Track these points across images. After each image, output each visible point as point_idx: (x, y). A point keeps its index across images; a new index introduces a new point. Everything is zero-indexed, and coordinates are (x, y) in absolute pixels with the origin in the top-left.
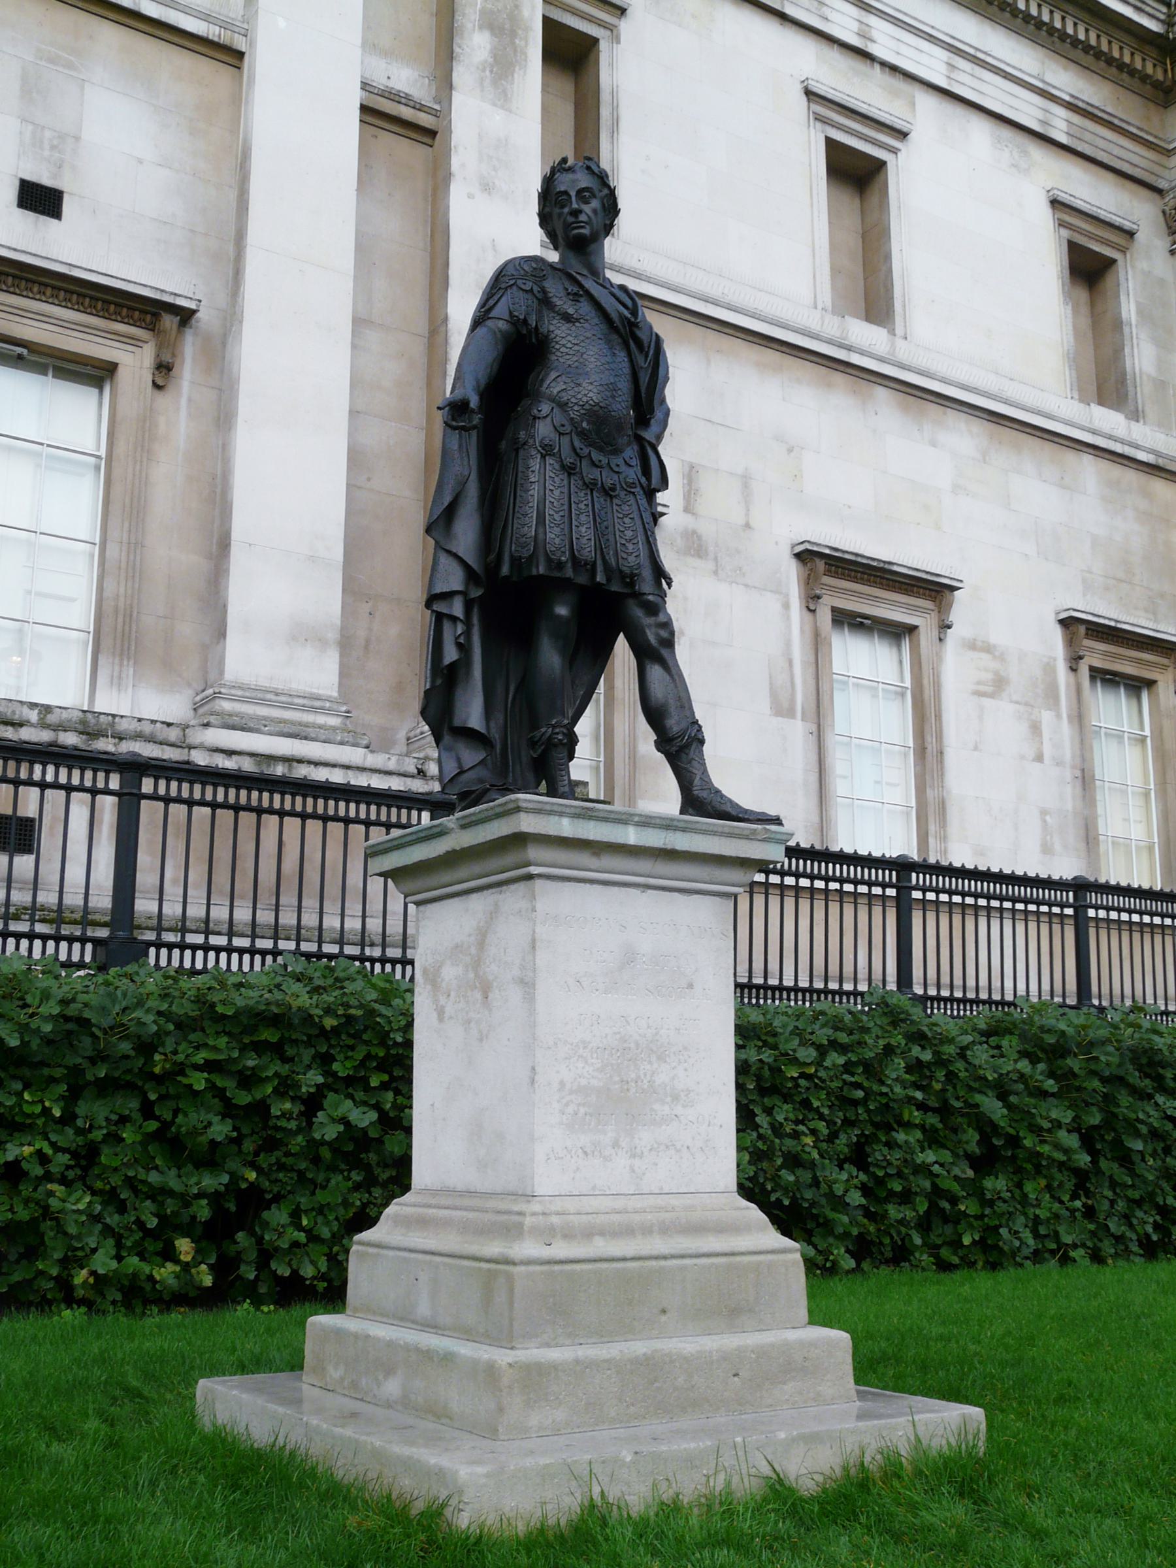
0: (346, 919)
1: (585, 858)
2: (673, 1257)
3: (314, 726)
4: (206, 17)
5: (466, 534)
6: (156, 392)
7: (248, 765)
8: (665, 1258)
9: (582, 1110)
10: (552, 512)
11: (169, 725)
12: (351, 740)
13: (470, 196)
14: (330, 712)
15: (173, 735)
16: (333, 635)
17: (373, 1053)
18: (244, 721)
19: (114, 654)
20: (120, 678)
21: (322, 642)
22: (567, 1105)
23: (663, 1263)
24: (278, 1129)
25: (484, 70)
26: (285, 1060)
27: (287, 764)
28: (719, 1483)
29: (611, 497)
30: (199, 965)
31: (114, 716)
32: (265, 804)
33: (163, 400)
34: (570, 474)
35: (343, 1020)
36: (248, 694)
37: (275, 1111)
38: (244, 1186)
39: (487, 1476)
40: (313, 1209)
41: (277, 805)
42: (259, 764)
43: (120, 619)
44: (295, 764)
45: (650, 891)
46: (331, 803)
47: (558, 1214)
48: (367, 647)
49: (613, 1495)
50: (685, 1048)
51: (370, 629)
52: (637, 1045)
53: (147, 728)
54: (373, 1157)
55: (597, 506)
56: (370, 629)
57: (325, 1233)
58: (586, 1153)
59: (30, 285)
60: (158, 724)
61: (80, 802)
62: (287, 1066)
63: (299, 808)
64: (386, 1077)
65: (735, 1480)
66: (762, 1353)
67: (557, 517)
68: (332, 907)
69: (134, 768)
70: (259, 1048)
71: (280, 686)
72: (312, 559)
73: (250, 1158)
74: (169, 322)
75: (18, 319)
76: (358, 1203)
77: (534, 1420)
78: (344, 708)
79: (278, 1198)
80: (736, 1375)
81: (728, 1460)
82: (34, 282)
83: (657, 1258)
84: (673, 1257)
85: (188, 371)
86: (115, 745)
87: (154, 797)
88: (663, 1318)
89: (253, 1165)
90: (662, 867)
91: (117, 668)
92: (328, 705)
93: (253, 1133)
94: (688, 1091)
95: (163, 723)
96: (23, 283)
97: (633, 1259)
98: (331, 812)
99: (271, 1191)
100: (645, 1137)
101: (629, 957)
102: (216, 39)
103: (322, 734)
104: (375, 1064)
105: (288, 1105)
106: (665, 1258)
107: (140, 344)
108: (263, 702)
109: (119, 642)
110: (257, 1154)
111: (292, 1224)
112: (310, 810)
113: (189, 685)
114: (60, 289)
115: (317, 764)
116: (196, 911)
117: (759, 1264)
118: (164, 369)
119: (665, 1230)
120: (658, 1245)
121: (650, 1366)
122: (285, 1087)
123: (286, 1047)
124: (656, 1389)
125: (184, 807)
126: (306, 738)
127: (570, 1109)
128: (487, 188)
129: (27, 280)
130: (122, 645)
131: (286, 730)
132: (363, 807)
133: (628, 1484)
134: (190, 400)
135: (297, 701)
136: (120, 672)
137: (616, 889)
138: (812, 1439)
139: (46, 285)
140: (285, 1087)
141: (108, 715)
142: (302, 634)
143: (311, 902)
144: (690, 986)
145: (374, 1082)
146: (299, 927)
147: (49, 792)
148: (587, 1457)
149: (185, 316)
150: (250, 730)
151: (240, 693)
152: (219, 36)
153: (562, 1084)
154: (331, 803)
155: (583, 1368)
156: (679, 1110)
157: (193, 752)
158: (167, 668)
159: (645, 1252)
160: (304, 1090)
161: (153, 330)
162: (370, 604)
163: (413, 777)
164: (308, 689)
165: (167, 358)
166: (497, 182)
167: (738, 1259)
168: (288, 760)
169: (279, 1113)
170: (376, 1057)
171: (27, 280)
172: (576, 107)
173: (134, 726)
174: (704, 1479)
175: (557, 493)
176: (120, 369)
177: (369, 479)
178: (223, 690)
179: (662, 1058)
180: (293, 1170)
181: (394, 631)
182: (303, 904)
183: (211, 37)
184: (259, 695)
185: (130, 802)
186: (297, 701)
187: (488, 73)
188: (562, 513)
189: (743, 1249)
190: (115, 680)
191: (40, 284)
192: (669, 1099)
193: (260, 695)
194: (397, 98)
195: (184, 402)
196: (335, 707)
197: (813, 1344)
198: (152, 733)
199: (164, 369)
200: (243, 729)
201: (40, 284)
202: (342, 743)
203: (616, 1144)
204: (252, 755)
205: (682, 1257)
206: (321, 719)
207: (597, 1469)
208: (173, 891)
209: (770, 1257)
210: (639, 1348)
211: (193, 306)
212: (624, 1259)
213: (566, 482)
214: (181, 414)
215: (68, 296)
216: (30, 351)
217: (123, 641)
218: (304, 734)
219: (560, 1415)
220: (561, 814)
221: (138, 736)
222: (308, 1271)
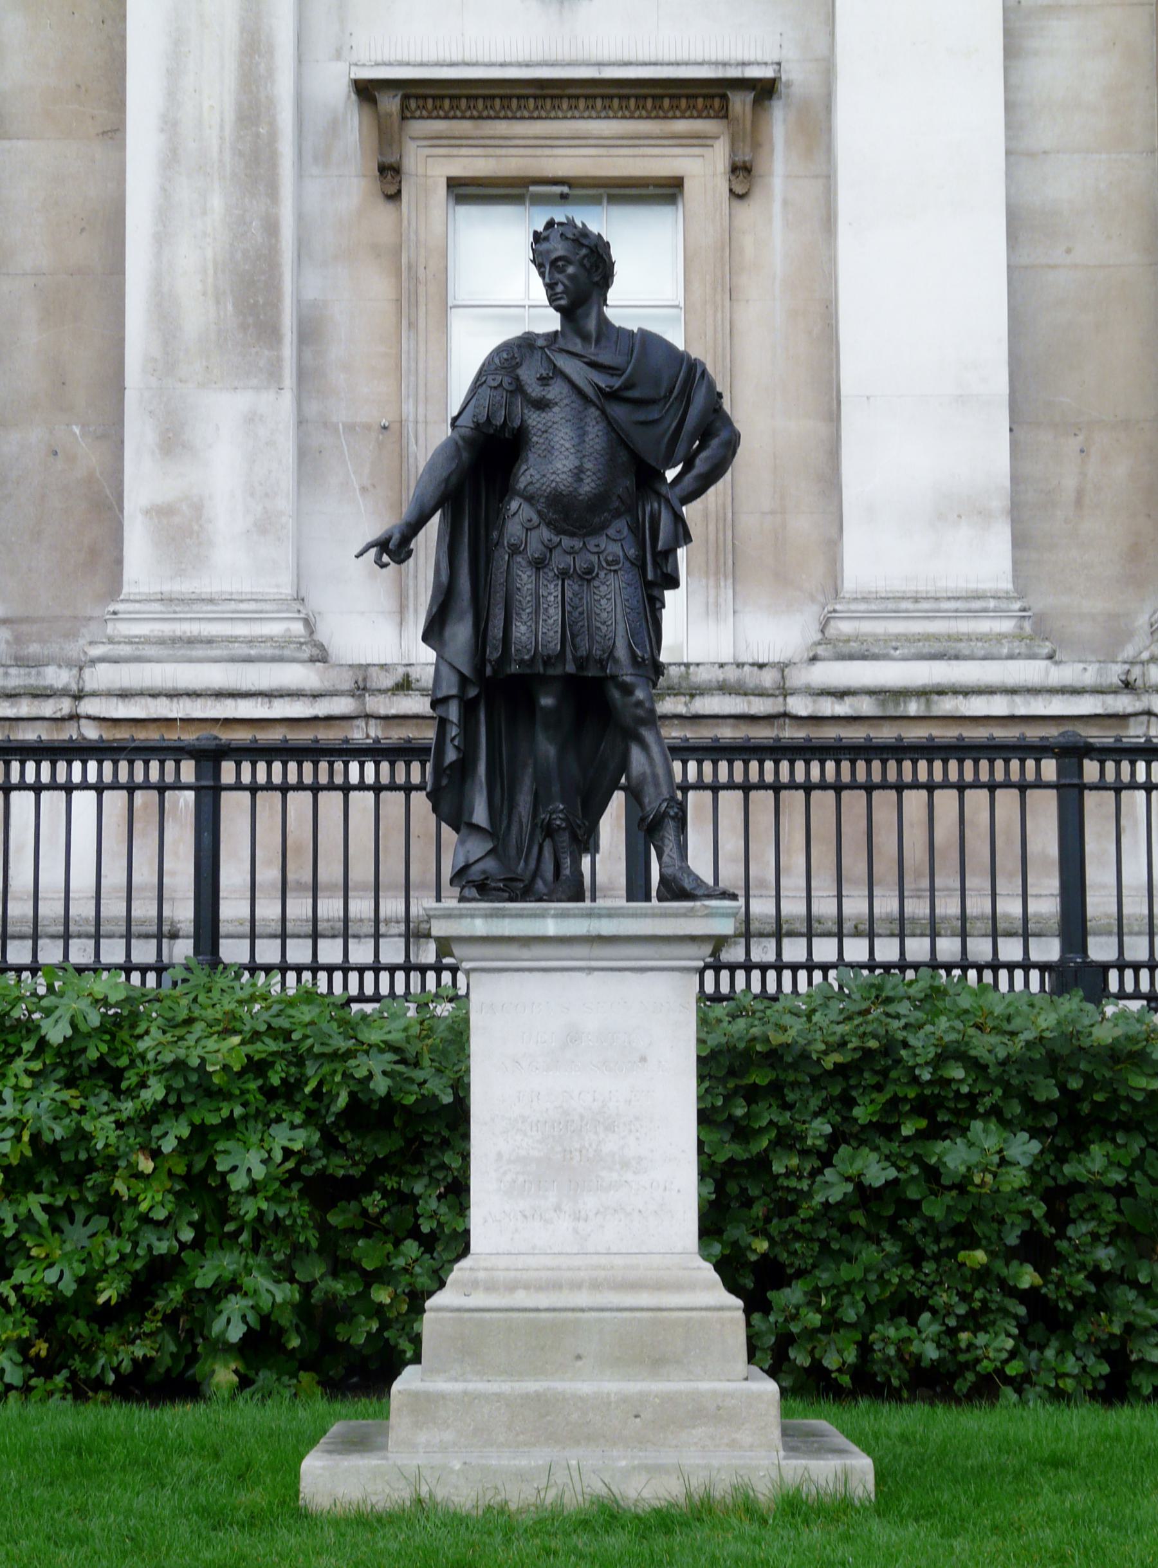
0: (1030, 900)
1: (513, 950)
2: (591, 1309)
3: (969, 638)
5: (461, 632)
6: (736, 204)
8: (582, 1310)
9: (521, 1179)
11: (761, 666)
12: (1023, 650)
14: (998, 613)
15: (768, 679)
16: (1000, 502)
17: (901, 1095)
18: (865, 647)
19: (707, 574)
20: (717, 604)
21: (984, 515)
22: (505, 1173)
23: (579, 1315)
24: (789, 1190)
26: (787, 1106)
27: (923, 700)
28: (550, 1496)
29: (589, 581)
30: (725, 989)
31: (687, 665)
33: (747, 213)
34: (538, 569)
35: (857, 1055)
36: (873, 607)
37: (778, 1168)
38: (753, 1258)
39: (323, 1468)
40: (833, 1286)
42: (883, 704)
43: (712, 527)
44: (935, 698)
45: (596, 973)
47: (486, 1269)
48: (1079, 502)
49: (440, 1494)
50: (637, 1119)
52: (582, 1117)
53: (732, 674)
54: (916, 1224)
57: (850, 1315)
58: (525, 1217)
59: (556, 102)
60: (747, 668)
61: (84, 801)
62: (788, 1114)
64: (923, 1124)
65: (567, 1496)
66: (669, 1399)
68: (1008, 886)
70: (752, 1094)
71: (922, 587)
73: (760, 1225)
74: (740, 103)
75: (547, 151)
76: (896, 1280)
77: (422, 1437)
78: (1017, 605)
79: (800, 1274)
80: (636, 1416)
81: (560, 1477)
82: (561, 97)
83: (573, 1310)
84: (591, 1309)
85: (780, 164)
86: (686, 704)
88: (579, 1363)
89: (765, 1234)
90: (598, 950)
91: (712, 592)
92: (992, 604)
93: (765, 1193)
94: (640, 1159)
95: (753, 665)
96: (548, 102)
97: (547, 1310)
99: (792, 1265)
100: (590, 1202)
101: (573, 1037)
103: (979, 648)
104: (908, 1107)
105: (794, 1161)
106: (582, 1310)
107: (709, 142)
108: (897, 615)
109: (712, 556)
110: (768, 1220)
111: (809, 1304)
113: (813, 599)
114: (594, 97)
115: (966, 692)
116: (825, 907)
117: (689, 1319)
118: (743, 174)
119: (596, 1286)
120: (582, 1299)
121: (542, 1403)
122: (787, 1139)
123: (786, 1091)
124: (544, 1418)
126: (957, 657)
127: (508, 1177)
129: (552, 97)
130: (717, 560)
131: (926, 650)
133: (456, 1487)
134: (785, 202)
135: (945, 605)
136: (717, 596)
137: (558, 975)
138: (655, 1470)
139: (577, 97)
140: (787, 1139)
141: (680, 664)
142: (953, 510)
143: (977, 882)
144: (643, 1059)
145: (907, 1130)
146: (963, 917)
148: (415, 1463)
149: (764, 91)
150: (875, 657)
151: (862, 606)
153: (499, 1155)
155: (470, 1400)
156: (629, 1176)
157: (791, 700)
158: (782, 580)
159: (559, 1305)
160: (809, 1142)
161: (726, 117)
162: (1081, 438)
163: (1115, 692)
164: (962, 584)
165: (745, 156)
167: (665, 1314)
168: (925, 693)
169: (783, 1171)
170: (905, 1099)
171: (552, 97)
173: (719, 675)
174: (535, 1492)
176: (687, 185)
177: (1068, 251)
178: (838, 607)
179: (610, 1128)
180: (812, 1240)
181: (1121, 469)
182: (967, 885)
184: (890, 604)
186: (945, 605)
189: (673, 1305)
190: (712, 608)
191: (569, 97)
192: (618, 1166)
193: (891, 605)
195: (777, 207)
196: (1003, 605)
197: (726, 1395)
198: (739, 681)
199: (743, 174)
200: (864, 657)
201: (569, 97)
202: (1011, 657)
203: (558, 1208)
204: (871, 692)
205: (602, 1310)
206: (984, 626)
207: (424, 1472)
208: (794, 882)
209: (704, 1314)
210: (532, 1386)
211: (768, 73)
212: (537, 1310)
214: (771, 227)
215: (607, 102)
216: (570, 186)
217: (717, 554)
218: (952, 652)
219: (448, 1436)
220: (472, 916)
221: (724, 688)
222: (831, 1362)
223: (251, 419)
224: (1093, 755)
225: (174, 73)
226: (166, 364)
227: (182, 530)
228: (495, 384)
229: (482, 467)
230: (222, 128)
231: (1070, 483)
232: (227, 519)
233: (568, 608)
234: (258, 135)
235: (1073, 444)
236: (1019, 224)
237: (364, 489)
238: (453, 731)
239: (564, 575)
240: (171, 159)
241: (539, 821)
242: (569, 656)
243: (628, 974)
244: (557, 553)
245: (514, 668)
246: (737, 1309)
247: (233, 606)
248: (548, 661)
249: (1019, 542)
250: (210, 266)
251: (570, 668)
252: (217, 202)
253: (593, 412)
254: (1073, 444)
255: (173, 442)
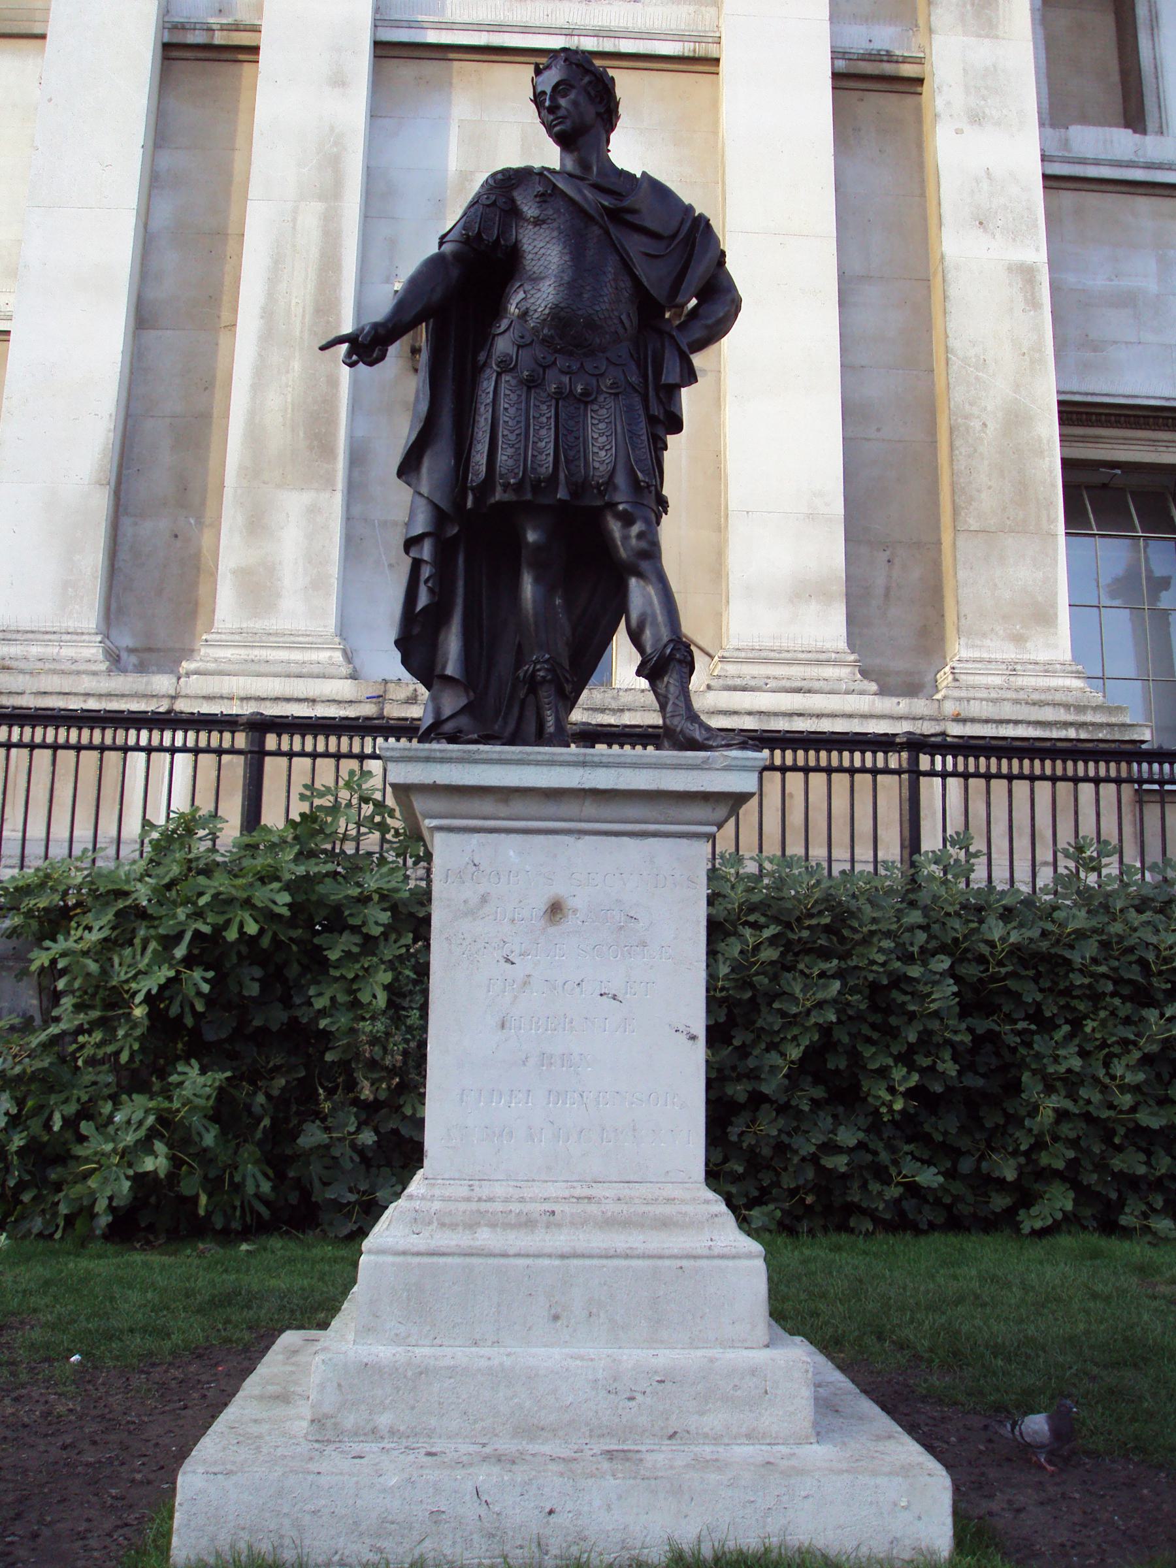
1: (487, 806)
4: (680, 38)
7: (749, 723)
10: (506, 433)
13: (959, 132)
14: (836, 663)
16: (840, 587)
25: (964, 6)
32: (994, 770)
34: (529, 388)
41: (1005, 770)
46: (846, 754)
48: (887, 595)
51: (889, 577)
55: (562, 415)
56: (889, 577)
63: (1005, 770)
67: (512, 437)
69: (260, 726)
72: (812, 517)
87: (278, 753)
98: (812, 763)
102: (691, 54)
112: (1059, 772)
125: (869, 777)
126: (809, 691)
128: (976, 118)
132: (1015, 762)
142: (804, 591)
147: (857, 776)
152: (694, 51)
154: (835, 754)
162: (888, 553)
166: (987, 111)
172: (1116, 14)
175: (512, 411)
177: (878, 430)
183: (686, 54)
185: (256, 758)
187: (969, 7)
188: (517, 432)
194: (878, 58)
202: (847, 693)
212: (505, 1255)
213: (523, 398)
223: (313, 510)
224: (926, 750)
225: (273, 281)
226: (253, 472)
227: (259, 589)
228: (488, 202)
229: (450, 313)
230: (304, 316)
231: (880, 581)
232: (292, 575)
233: (562, 431)
234: (328, 322)
235: (883, 556)
236: (851, 412)
237: (391, 566)
238: (426, 572)
239: (559, 396)
240: (267, 336)
241: (521, 674)
242: (562, 476)
243: (625, 839)
244: (551, 374)
245: (499, 495)
246: (750, 1256)
247: (292, 639)
248: (536, 486)
249: (852, 620)
250: (290, 407)
251: (562, 494)
252: (296, 365)
253: (596, 231)
254: (883, 556)
255: (257, 525)
